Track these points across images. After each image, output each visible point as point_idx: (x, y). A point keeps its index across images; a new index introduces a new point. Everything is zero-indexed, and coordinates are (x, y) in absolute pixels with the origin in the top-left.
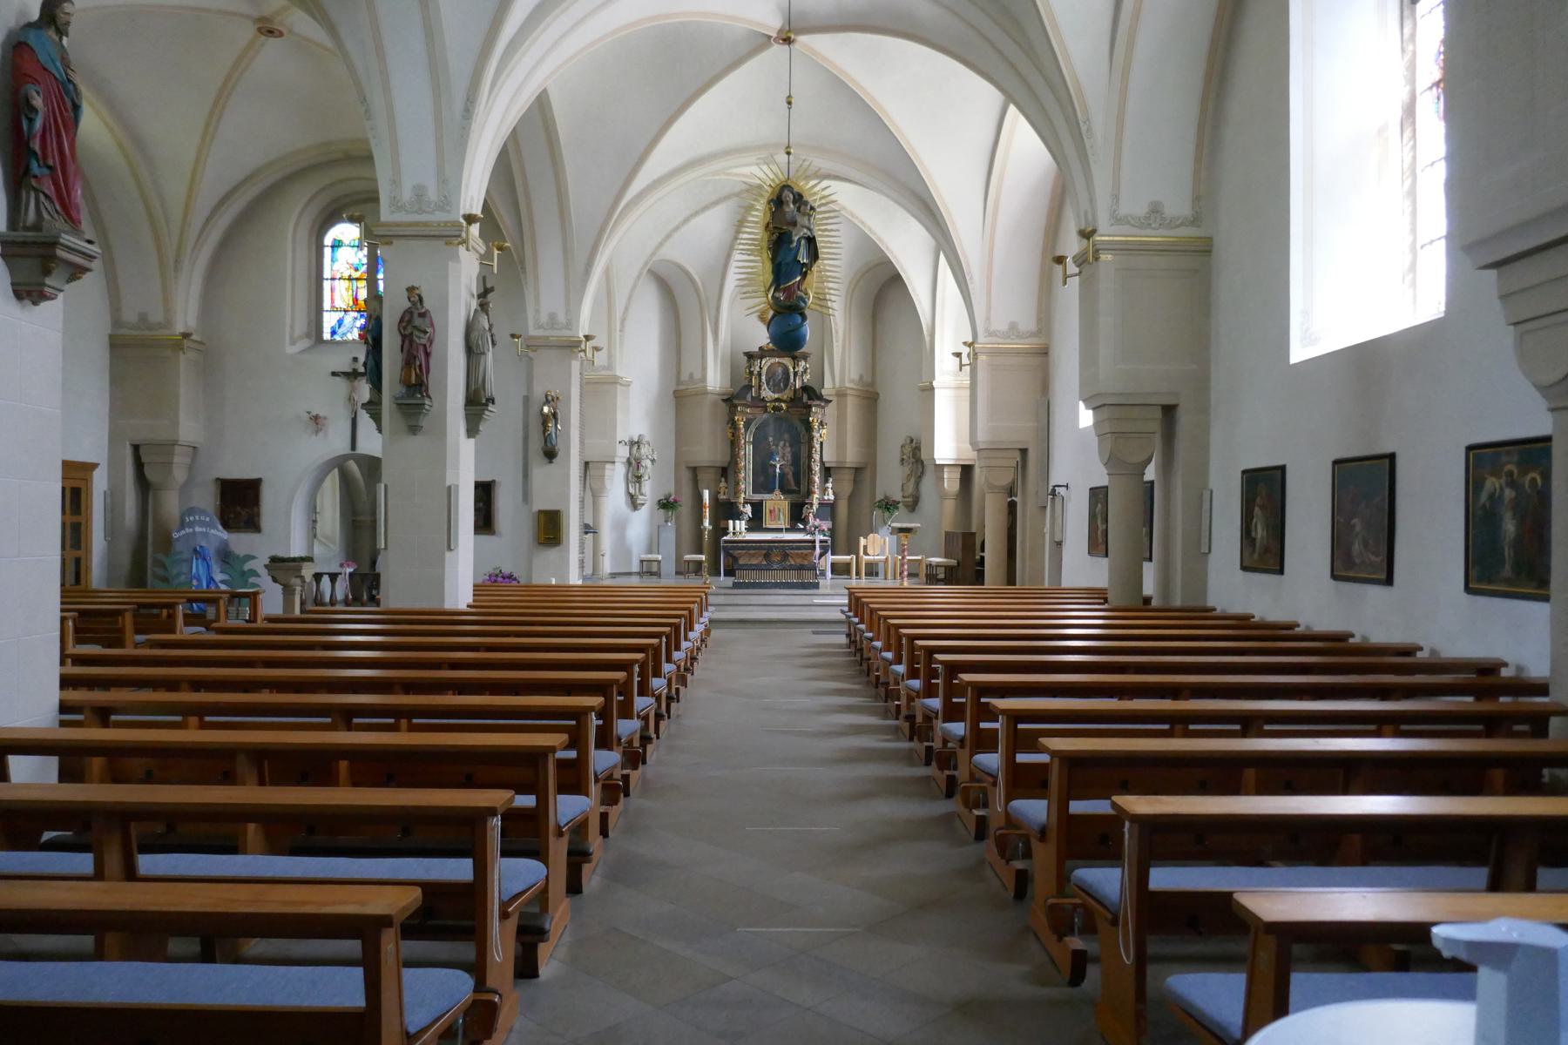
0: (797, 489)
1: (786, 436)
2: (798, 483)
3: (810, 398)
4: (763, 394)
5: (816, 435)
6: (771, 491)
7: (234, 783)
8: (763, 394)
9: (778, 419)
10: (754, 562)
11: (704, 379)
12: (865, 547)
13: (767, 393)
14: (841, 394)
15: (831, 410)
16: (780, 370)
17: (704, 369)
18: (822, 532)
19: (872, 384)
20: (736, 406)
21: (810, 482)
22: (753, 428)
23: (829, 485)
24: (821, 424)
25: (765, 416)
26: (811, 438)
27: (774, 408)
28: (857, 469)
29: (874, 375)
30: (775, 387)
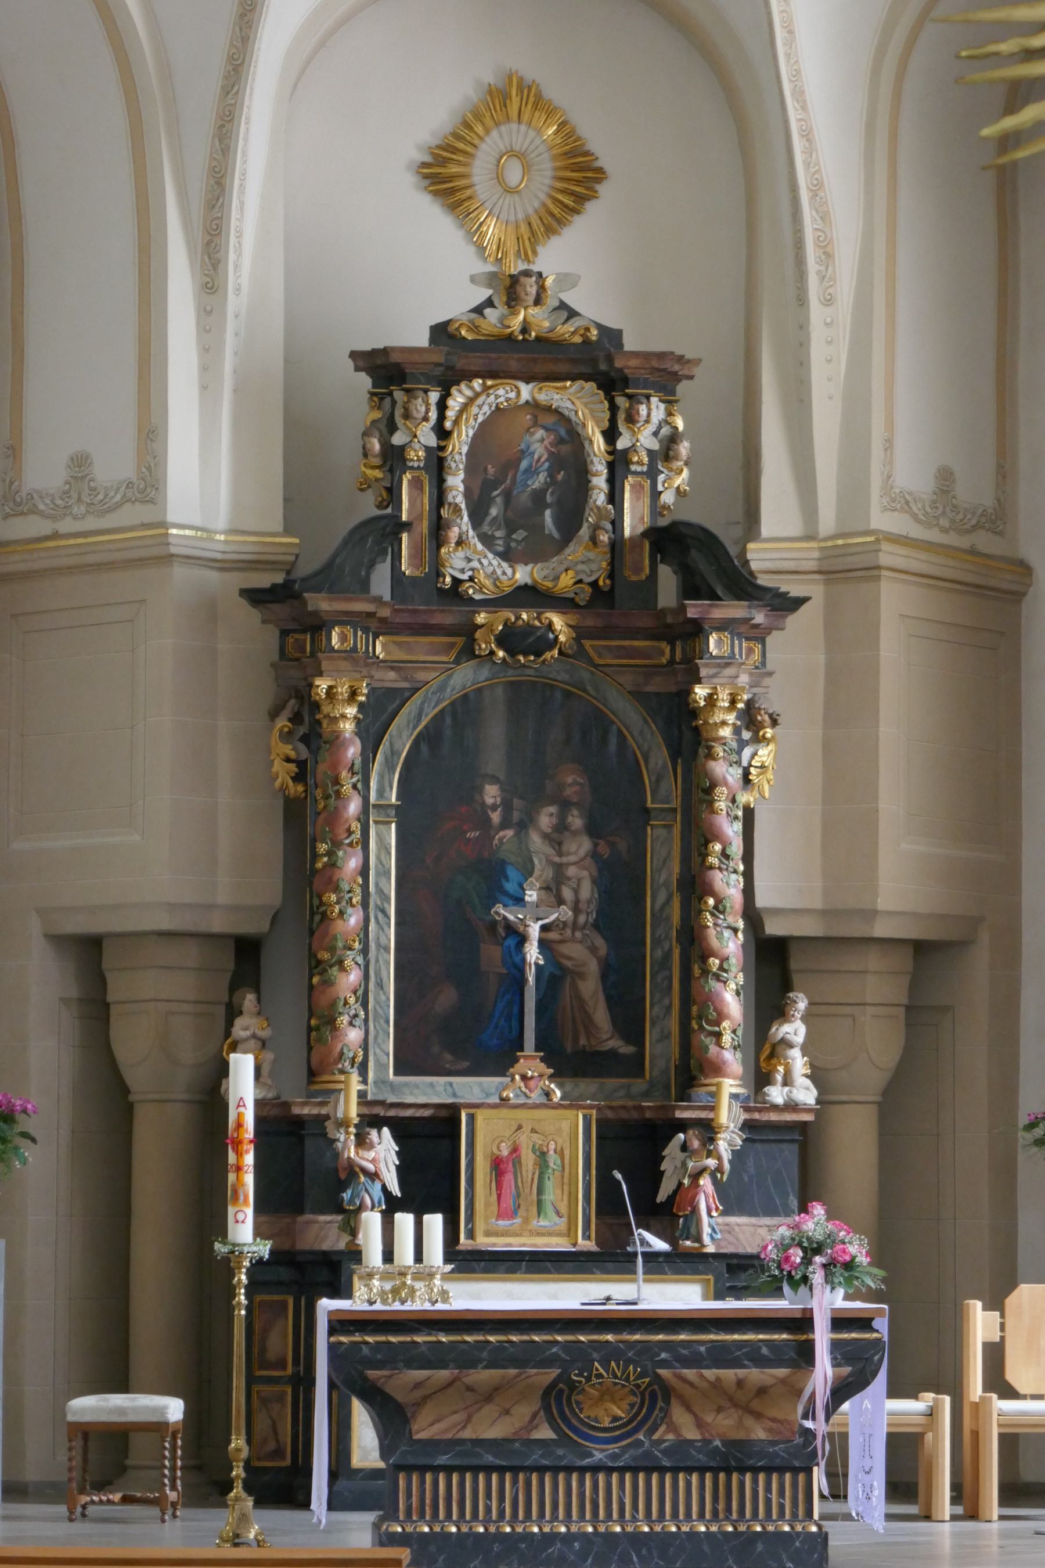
0: (629, 1053)
1: (572, 781)
2: (630, 1022)
3: (693, 588)
4: (456, 563)
5: (725, 771)
6: (499, 1060)
7: (916, 1484)
8: (456, 563)
9: (528, 699)
10: (491, 1426)
11: (149, 484)
12: (995, 1354)
13: (474, 562)
14: (848, 569)
15: (795, 648)
16: (539, 443)
17: (150, 435)
18: (841, 1269)
19: (997, 519)
20: (317, 626)
21: (696, 1012)
22: (401, 737)
23: (794, 1030)
24: (751, 719)
25: (464, 677)
26: (700, 792)
27: (512, 639)
28: (920, 949)
29: (1004, 471)
30: (518, 537)
